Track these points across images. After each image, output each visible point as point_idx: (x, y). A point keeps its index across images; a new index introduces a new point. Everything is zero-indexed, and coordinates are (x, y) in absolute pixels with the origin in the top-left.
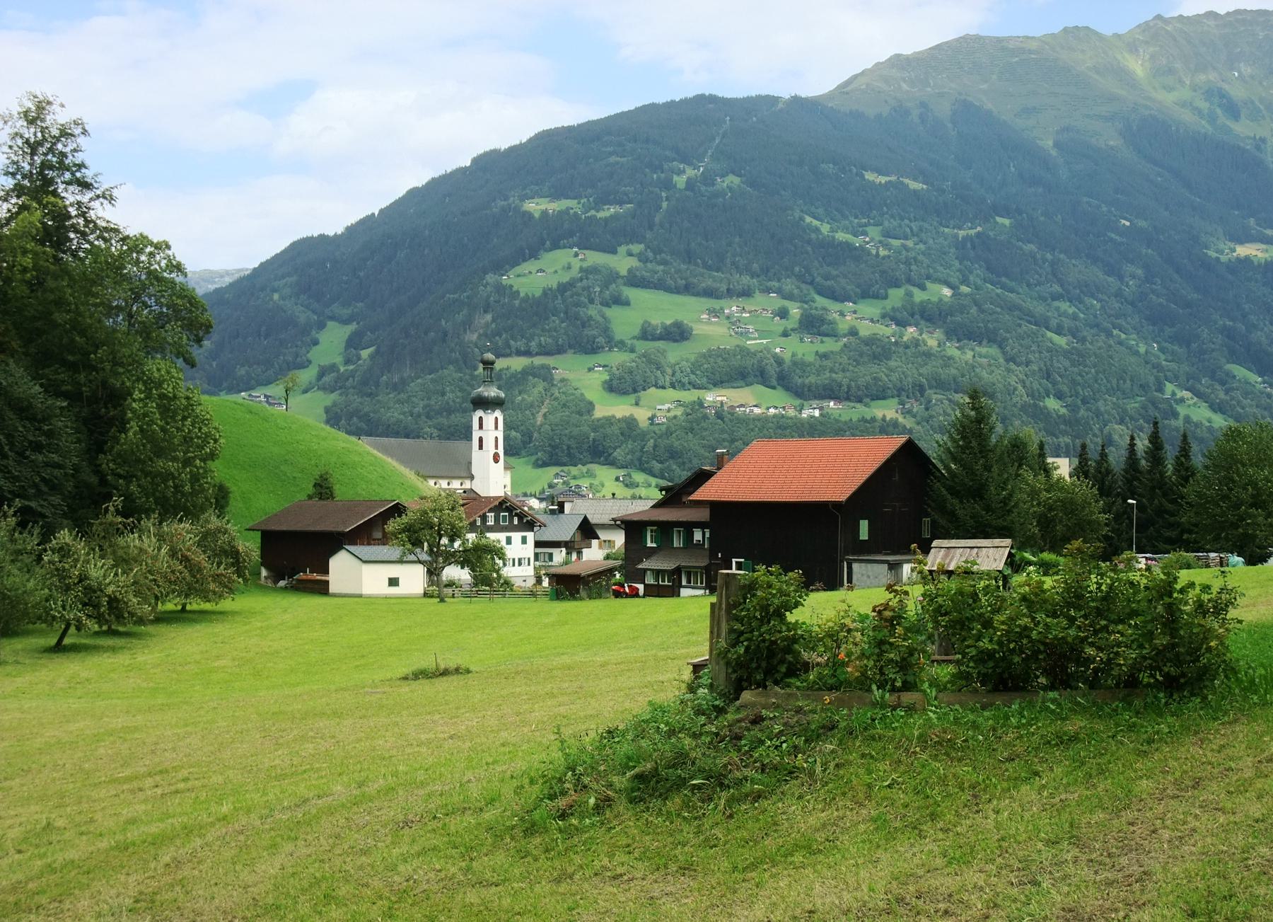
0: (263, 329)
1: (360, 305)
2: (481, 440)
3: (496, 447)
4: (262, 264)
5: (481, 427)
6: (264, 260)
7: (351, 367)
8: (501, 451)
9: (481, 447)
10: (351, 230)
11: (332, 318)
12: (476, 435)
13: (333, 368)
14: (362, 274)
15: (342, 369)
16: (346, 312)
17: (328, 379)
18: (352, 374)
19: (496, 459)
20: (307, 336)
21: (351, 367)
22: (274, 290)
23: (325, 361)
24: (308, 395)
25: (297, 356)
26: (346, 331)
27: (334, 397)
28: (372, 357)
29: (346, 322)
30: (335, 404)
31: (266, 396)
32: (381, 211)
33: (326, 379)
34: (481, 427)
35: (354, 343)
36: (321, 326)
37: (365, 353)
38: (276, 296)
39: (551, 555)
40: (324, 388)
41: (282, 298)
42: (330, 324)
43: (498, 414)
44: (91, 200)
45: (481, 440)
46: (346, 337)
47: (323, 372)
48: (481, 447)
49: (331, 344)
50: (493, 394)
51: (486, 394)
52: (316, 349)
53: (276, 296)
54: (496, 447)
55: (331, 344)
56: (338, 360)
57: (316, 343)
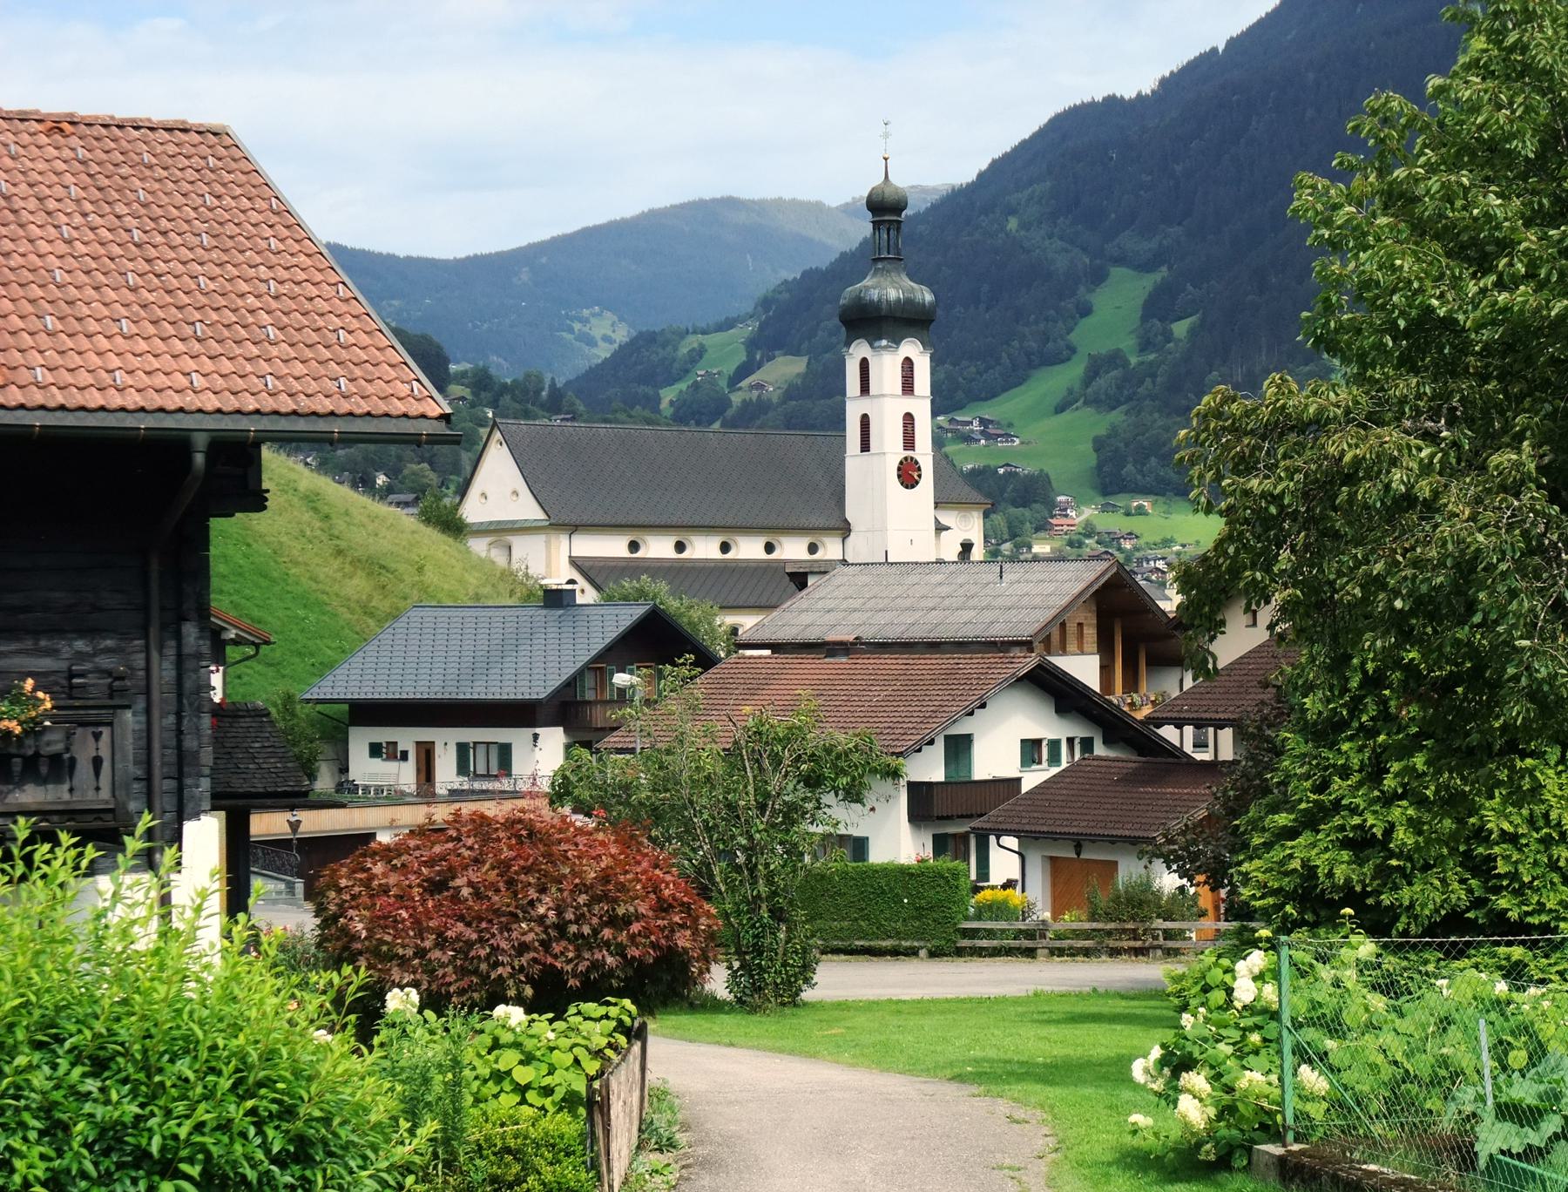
0: (985, 288)
1: (1175, 230)
2: (865, 422)
3: (909, 442)
4: (994, 163)
5: (865, 389)
6: (997, 154)
7: (1152, 357)
8: (924, 453)
9: (865, 446)
10: (1169, 85)
11: (1120, 261)
12: (854, 410)
13: (1115, 359)
14: (1178, 168)
15: (1133, 360)
16: (1144, 247)
17: (1108, 383)
18: (1151, 371)
19: (908, 475)
20: (1069, 298)
21: (1152, 357)
22: (1012, 211)
23: (1103, 347)
24: (1066, 416)
25: (1046, 338)
26: (1146, 283)
27: (1117, 416)
28: (1192, 332)
29: (1145, 267)
30: (1114, 432)
31: (983, 421)
32: (1231, 43)
33: (1101, 383)
34: (865, 389)
35: (1159, 308)
36: (1098, 277)
37: (1180, 328)
38: (1013, 224)
39: (505, 751)
40: (1095, 402)
41: (1025, 226)
42: (1117, 272)
43: (911, 348)
44: (1360, 237)
45: (865, 422)
46: (1145, 296)
47: (1096, 368)
48: (865, 446)
49: (1114, 312)
50: (893, 294)
51: (875, 295)
52: (1085, 323)
53: (1013, 224)
54: (909, 442)
55: (1114, 312)
56: (1127, 344)
57: (1086, 311)
